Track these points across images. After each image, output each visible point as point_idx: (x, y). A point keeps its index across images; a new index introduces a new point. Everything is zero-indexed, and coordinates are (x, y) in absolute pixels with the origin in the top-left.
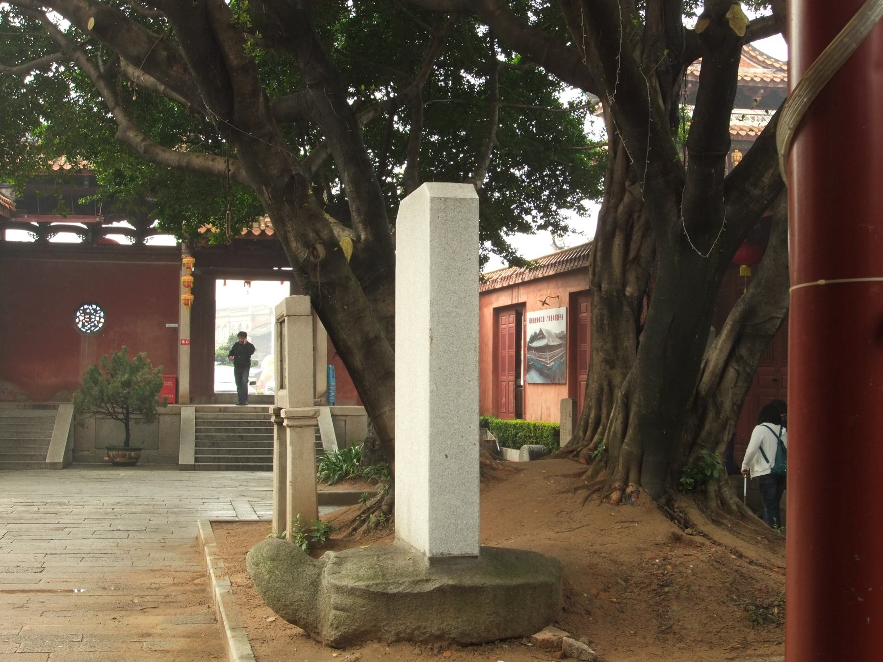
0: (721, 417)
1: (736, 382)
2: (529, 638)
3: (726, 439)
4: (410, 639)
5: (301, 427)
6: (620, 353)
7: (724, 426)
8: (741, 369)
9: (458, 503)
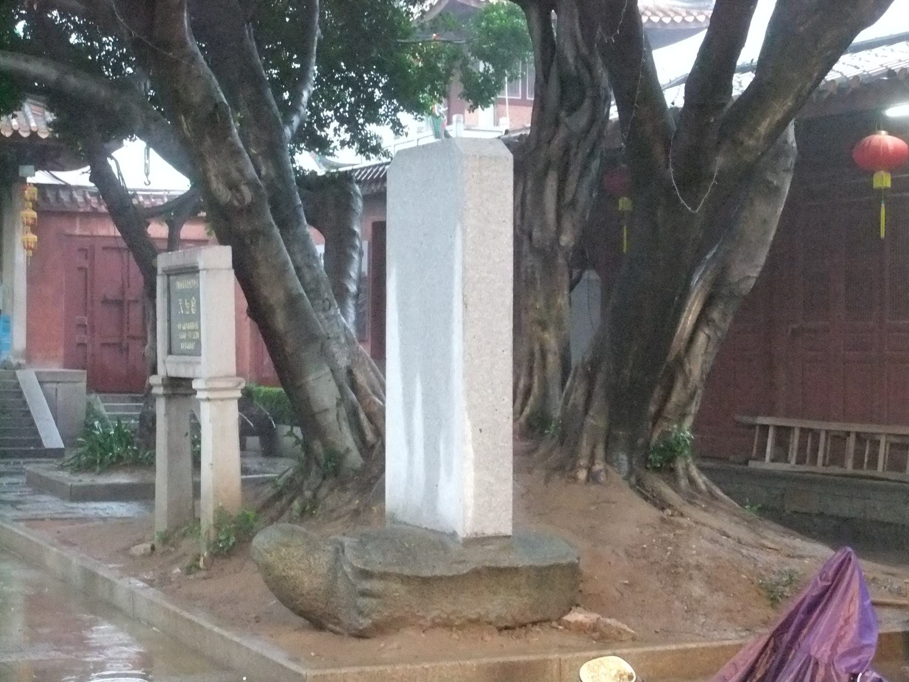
0: (689, 386)
1: (706, 349)
2: (559, 620)
3: (693, 411)
4: (447, 625)
5: (222, 400)
6: (554, 312)
7: (692, 397)
8: (712, 335)
9: (492, 480)
